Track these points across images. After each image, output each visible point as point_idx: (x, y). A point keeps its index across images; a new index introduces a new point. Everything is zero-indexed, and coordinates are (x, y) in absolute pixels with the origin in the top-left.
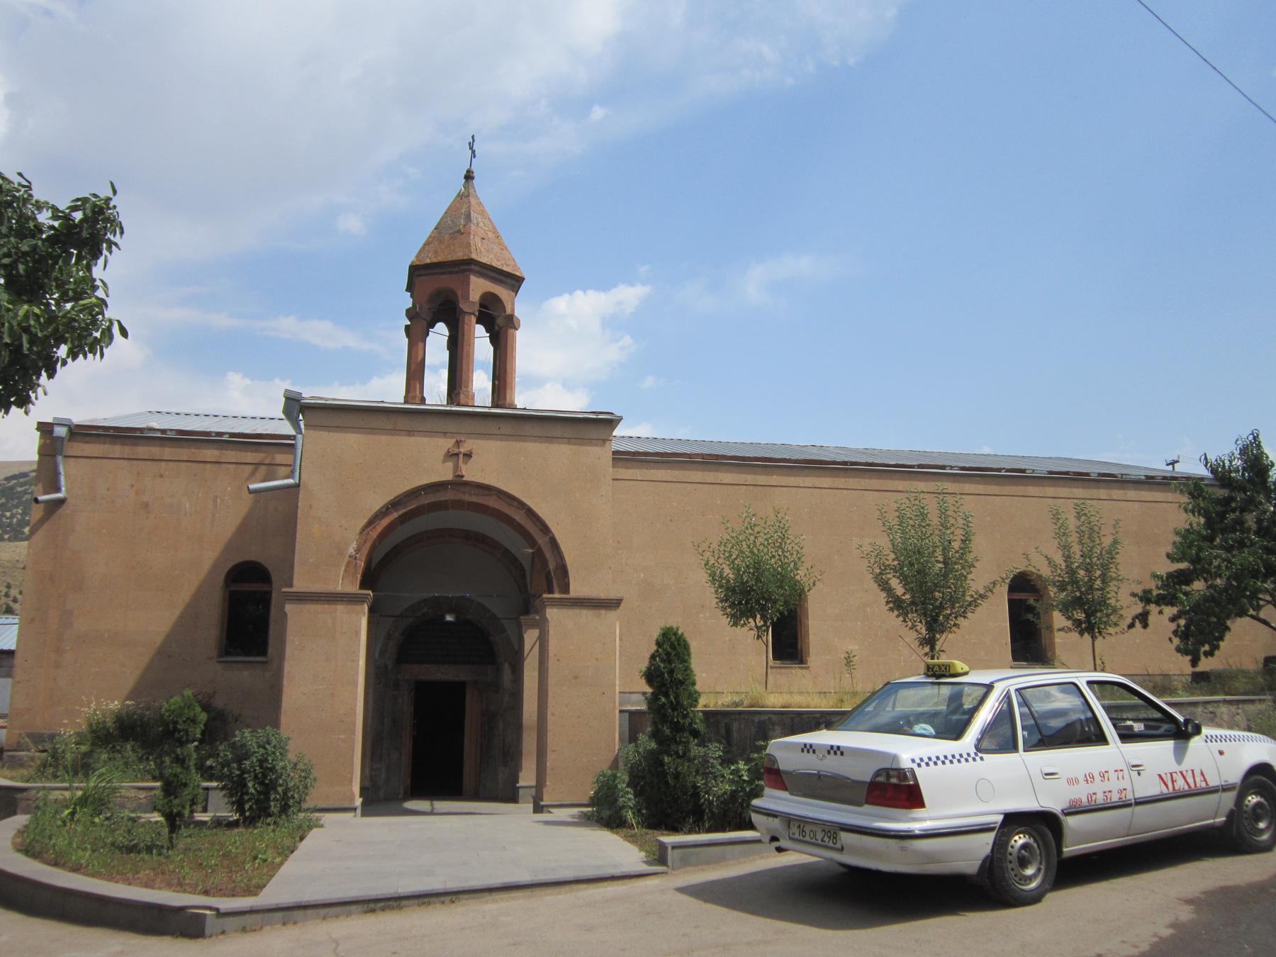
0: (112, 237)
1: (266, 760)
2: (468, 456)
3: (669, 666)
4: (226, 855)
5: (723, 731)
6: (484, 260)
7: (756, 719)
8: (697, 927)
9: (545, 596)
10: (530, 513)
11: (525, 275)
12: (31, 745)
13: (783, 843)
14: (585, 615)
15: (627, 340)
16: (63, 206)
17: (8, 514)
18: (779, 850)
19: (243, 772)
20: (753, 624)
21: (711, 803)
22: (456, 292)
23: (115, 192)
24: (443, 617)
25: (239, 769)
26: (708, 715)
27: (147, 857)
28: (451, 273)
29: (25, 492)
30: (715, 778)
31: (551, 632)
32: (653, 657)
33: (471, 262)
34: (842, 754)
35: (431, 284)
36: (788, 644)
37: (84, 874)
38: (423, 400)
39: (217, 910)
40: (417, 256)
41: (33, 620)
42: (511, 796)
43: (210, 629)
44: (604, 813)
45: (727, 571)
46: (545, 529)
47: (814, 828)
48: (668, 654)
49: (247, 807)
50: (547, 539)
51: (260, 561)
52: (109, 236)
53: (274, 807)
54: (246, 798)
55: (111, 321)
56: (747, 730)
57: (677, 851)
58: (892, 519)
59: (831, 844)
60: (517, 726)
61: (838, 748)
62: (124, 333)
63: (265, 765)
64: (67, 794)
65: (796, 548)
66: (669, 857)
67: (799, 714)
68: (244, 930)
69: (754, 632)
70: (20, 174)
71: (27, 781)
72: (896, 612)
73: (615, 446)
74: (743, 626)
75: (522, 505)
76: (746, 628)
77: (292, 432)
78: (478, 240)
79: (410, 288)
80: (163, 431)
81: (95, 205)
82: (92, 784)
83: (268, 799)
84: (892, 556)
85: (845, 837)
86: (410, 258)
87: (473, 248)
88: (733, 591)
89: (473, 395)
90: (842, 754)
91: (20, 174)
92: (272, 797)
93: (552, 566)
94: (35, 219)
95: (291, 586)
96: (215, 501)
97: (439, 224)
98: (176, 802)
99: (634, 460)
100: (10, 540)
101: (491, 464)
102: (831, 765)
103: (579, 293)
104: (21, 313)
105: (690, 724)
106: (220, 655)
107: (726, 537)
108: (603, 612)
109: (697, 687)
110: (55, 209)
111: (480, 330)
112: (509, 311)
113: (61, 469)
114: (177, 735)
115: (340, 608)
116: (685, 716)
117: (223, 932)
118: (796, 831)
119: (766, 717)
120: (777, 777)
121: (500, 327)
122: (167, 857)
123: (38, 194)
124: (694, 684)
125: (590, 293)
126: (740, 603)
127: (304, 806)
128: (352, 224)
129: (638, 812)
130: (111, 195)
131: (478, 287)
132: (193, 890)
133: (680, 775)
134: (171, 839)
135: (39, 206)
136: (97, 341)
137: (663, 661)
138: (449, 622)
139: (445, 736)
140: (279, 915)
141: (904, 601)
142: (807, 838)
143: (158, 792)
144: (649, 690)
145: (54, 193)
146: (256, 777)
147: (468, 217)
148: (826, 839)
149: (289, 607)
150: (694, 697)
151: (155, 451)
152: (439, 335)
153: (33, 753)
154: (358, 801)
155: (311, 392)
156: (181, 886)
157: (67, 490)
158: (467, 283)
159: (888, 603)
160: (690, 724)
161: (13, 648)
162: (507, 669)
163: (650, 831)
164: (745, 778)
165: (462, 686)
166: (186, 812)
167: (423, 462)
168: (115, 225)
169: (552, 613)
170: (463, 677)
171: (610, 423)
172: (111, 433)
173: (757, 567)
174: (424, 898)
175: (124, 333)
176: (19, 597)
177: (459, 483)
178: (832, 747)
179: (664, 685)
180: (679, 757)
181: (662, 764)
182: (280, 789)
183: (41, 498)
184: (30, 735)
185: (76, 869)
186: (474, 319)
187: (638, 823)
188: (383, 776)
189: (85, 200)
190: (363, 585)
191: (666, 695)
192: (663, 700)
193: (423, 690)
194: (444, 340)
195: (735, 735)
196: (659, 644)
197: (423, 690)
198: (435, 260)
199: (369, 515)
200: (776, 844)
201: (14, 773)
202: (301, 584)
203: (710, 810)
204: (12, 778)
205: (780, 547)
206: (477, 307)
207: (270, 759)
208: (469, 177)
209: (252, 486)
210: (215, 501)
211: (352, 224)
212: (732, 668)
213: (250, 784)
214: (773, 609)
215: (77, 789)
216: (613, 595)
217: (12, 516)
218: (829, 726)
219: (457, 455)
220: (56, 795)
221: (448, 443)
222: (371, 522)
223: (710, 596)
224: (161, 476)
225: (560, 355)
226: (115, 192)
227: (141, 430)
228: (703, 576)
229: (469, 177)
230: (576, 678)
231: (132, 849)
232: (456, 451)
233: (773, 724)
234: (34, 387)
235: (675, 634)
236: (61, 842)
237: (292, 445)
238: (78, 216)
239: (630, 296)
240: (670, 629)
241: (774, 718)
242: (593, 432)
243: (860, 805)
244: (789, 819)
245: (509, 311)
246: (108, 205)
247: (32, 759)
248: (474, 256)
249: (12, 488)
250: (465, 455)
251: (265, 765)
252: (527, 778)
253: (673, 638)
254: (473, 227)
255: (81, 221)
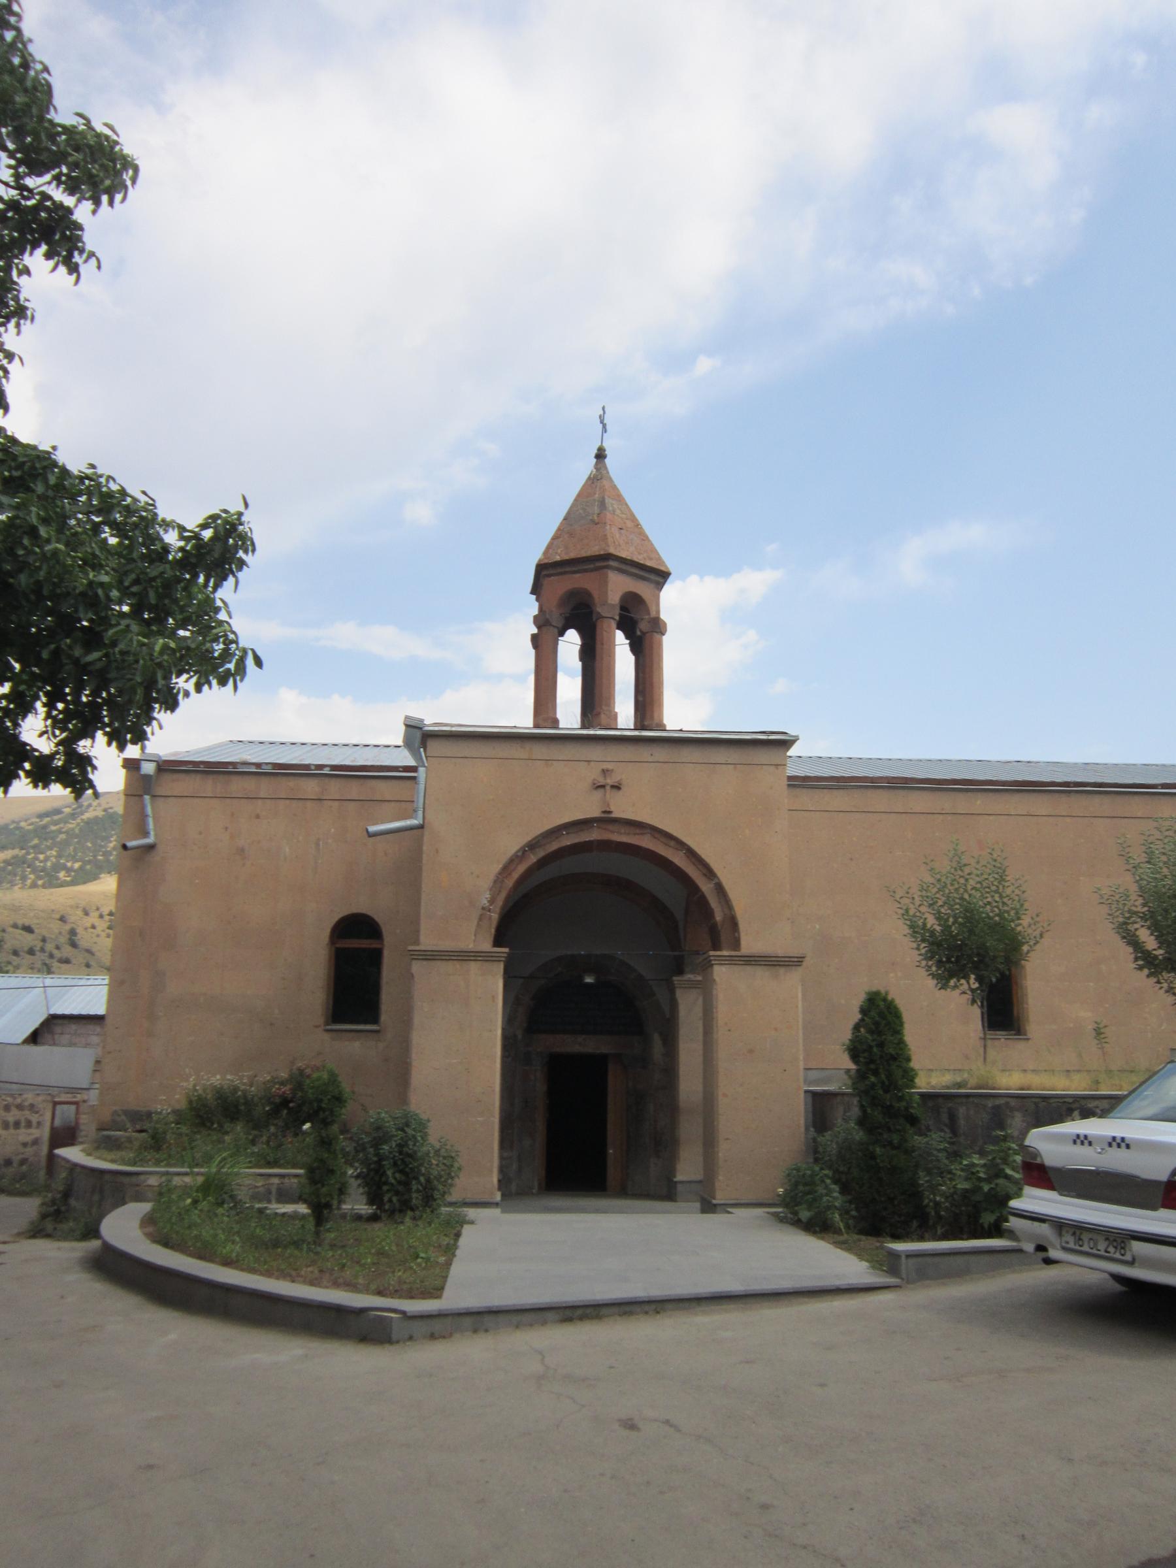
0: (244, 556)
1: (407, 1145)
2: (617, 787)
3: (878, 1034)
4: (381, 1253)
5: (945, 1118)
6: (623, 554)
7: (990, 1103)
8: (958, 1349)
9: (712, 953)
10: (691, 854)
11: (671, 570)
12: (128, 1125)
13: (1053, 1253)
14: (761, 975)
15: (752, 635)
16: (191, 524)
17: (41, 857)
18: (1048, 1261)
19: (381, 1159)
20: (966, 986)
21: (937, 1204)
22: (595, 591)
23: (246, 505)
24: (581, 978)
25: (377, 1155)
26: (925, 1097)
27: (296, 1252)
28: (585, 571)
29: (60, 832)
30: (941, 1174)
31: (721, 996)
32: (857, 1027)
33: (608, 557)
34: (1128, 1146)
35: (560, 586)
36: (1002, 1011)
37: (236, 1268)
38: (555, 723)
39: (404, 1313)
40: (546, 553)
41: (122, 983)
42: (665, 1191)
43: (315, 990)
44: (802, 1209)
45: (931, 921)
46: (709, 873)
47: (1095, 1236)
48: (877, 1024)
49: (386, 1199)
50: (712, 886)
51: (369, 913)
52: (241, 554)
53: (416, 1199)
54: (385, 1188)
55: (245, 651)
56: (995, 1119)
57: (912, 1261)
58: (1138, 856)
59: (1118, 1256)
60: (672, 1109)
61: (1123, 1139)
62: (259, 662)
63: (405, 1149)
64: (187, 1179)
65: (1017, 892)
66: (903, 1267)
67: (1045, 1098)
68: (433, 1337)
69: (969, 996)
70: (144, 493)
71: (134, 1164)
72: (1146, 971)
73: (792, 771)
74: (956, 987)
75: (680, 844)
76: (958, 991)
77: (411, 762)
78: (615, 530)
79: (536, 590)
80: (258, 765)
81: (226, 522)
82: (214, 1170)
83: (409, 1190)
84: (1140, 901)
85: (1137, 1247)
86: (535, 555)
87: (610, 540)
88: (939, 944)
89: (616, 715)
90: (1128, 1146)
91: (144, 493)
92: (414, 1187)
93: (718, 917)
94: (162, 540)
95: (417, 942)
96: (317, 844)
97: (569, 513)
98: (324, 1190)
99: (804, 787)
100: (44, 886)
101: (646, 798)
102: (1118, 1161)
103: (694, 578)
104: (157, 648)
105: (907, 1109)
106: (327, 1024)
107: (930, 880)
108: (782, 970)
109: (912, 1064)
110: (182, 529)
111: (620, 636)
112: (653, 614)
113: (149, 810)
114: (321, 1115)
115: (474, 966)
116: (901, 1099)
117: (411, 1338)
118: (1071, 1239)
119: (1001, 1101)
120: (1041, 1174)
121: (644, 634)
122: (317, 1253)
123: (163, 513)
124: (909, 1060)
125: (708, 579)
126: (949, 961)
127: (449, 1199)
128: (421, 513)
129: (845, 1212)
130: (242, 509)
131: (617, 586)
132: (366, 1290)
133: (898, 1170)
134: (317, 1233)
135: (166, 525)
136: (228, 673)
137: (871, 1032)
138: (588, 984)
139: (592, 1119)
140: (468, 1321)
141: (1156, 957)
142: (1086, 1248)
143: (303, 1180)
144: (853, 1066)
145: (183, 510)
146: (395, 1164)
147: (602, 504)
148: (1111, 1249)
149: (417, 967)
150: (909, 1076)
151: (249, 784)
152: (570, 644)
153: (130, 1133)
154: (498, 1197)
155: (434, 715)
156: (352, 1286)
157: (156, 835)
158: (604, 582)
159: (1136, 959)
160: (907, 1109)
161: (101, 1010)
162: (657, 1040)
163: (863, 1238)
164: (982, 1175)
165: (600, 1062)
166: (335, 1203)
167: (565, 797)
168: (246, 543)
169: (720, 973)
170: (604, 1050)
171: (784, 743)
172: (202, 768)
173: (970, 917)
174: (627, 1308)
175: (259, 662)
176: (55, 952)
177: (607, 820)
178: (1114, 1138)
179: (872, 1061)
180: (894, 1148)
181: (873, 1157)
182: (422, 1179)
183: (130, 844)
184: (126, 1112)
185: (227, 1263)
186: (614, 625)
187: (848, 1227)
188: (515, 1166)
189: (214, 517)
190: (497, 942)
191: (876, 1073)
192: (873, 1079)
193: (558, 1065)
194: (576, 649)
195: (962, 1122)
196: (864, 1011)
197: (558, 1065)
198: (567, 558)
199: (504, 859)
200: (1042, 1255)
201: (112, 1156)
202: (427, 941)
203: (937, 1213)
204: (113, 1161)
205: (996, 892)
206: (618, 611)
207: (410, 1143)
208: (600, 455)
209: (372, 829)
210: (317, 844)
211: (421, 513)
212: (945, 1042)
213: (389, 1173)
214: (983, 960)
215: (198, 1174)
216: (794, 952)
217: (47, 859)
218: (1086, 1114)
219: (603, 786)
220: (177, 1181)
221: (592, 774)
222: (506, 869)
223: (910, 953)
224: (258, 817)
225: (712, 664)
226: (246, 505)
227: (233, 764)
228: (899, 931)
229: (600, 455)
230: (751, 1051)
231: (276, 1243)
232: (602, 781)
233: (1012, 1109)
234: (149, 720)
235: (885, 1000)
236: (206, 1233)
237: (414, 778)
238: (207, 534)
239: (755, 582)
240: (877, 993)
241: (1013, 1102)
242: (763, 756)
243: (1154, 1209)
244: (1060, 1225)
245: (653, 614)
246: (239, 519)
247: (129, 1140)
248: (612, 550)
249: (45, 827)
250: (613, 787)
251: (405, 1149)
252: (687, 1169)
253: (882, 1004)
254: (609, 516)
255: (212, 539)
